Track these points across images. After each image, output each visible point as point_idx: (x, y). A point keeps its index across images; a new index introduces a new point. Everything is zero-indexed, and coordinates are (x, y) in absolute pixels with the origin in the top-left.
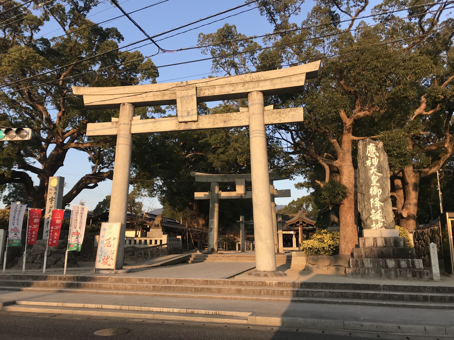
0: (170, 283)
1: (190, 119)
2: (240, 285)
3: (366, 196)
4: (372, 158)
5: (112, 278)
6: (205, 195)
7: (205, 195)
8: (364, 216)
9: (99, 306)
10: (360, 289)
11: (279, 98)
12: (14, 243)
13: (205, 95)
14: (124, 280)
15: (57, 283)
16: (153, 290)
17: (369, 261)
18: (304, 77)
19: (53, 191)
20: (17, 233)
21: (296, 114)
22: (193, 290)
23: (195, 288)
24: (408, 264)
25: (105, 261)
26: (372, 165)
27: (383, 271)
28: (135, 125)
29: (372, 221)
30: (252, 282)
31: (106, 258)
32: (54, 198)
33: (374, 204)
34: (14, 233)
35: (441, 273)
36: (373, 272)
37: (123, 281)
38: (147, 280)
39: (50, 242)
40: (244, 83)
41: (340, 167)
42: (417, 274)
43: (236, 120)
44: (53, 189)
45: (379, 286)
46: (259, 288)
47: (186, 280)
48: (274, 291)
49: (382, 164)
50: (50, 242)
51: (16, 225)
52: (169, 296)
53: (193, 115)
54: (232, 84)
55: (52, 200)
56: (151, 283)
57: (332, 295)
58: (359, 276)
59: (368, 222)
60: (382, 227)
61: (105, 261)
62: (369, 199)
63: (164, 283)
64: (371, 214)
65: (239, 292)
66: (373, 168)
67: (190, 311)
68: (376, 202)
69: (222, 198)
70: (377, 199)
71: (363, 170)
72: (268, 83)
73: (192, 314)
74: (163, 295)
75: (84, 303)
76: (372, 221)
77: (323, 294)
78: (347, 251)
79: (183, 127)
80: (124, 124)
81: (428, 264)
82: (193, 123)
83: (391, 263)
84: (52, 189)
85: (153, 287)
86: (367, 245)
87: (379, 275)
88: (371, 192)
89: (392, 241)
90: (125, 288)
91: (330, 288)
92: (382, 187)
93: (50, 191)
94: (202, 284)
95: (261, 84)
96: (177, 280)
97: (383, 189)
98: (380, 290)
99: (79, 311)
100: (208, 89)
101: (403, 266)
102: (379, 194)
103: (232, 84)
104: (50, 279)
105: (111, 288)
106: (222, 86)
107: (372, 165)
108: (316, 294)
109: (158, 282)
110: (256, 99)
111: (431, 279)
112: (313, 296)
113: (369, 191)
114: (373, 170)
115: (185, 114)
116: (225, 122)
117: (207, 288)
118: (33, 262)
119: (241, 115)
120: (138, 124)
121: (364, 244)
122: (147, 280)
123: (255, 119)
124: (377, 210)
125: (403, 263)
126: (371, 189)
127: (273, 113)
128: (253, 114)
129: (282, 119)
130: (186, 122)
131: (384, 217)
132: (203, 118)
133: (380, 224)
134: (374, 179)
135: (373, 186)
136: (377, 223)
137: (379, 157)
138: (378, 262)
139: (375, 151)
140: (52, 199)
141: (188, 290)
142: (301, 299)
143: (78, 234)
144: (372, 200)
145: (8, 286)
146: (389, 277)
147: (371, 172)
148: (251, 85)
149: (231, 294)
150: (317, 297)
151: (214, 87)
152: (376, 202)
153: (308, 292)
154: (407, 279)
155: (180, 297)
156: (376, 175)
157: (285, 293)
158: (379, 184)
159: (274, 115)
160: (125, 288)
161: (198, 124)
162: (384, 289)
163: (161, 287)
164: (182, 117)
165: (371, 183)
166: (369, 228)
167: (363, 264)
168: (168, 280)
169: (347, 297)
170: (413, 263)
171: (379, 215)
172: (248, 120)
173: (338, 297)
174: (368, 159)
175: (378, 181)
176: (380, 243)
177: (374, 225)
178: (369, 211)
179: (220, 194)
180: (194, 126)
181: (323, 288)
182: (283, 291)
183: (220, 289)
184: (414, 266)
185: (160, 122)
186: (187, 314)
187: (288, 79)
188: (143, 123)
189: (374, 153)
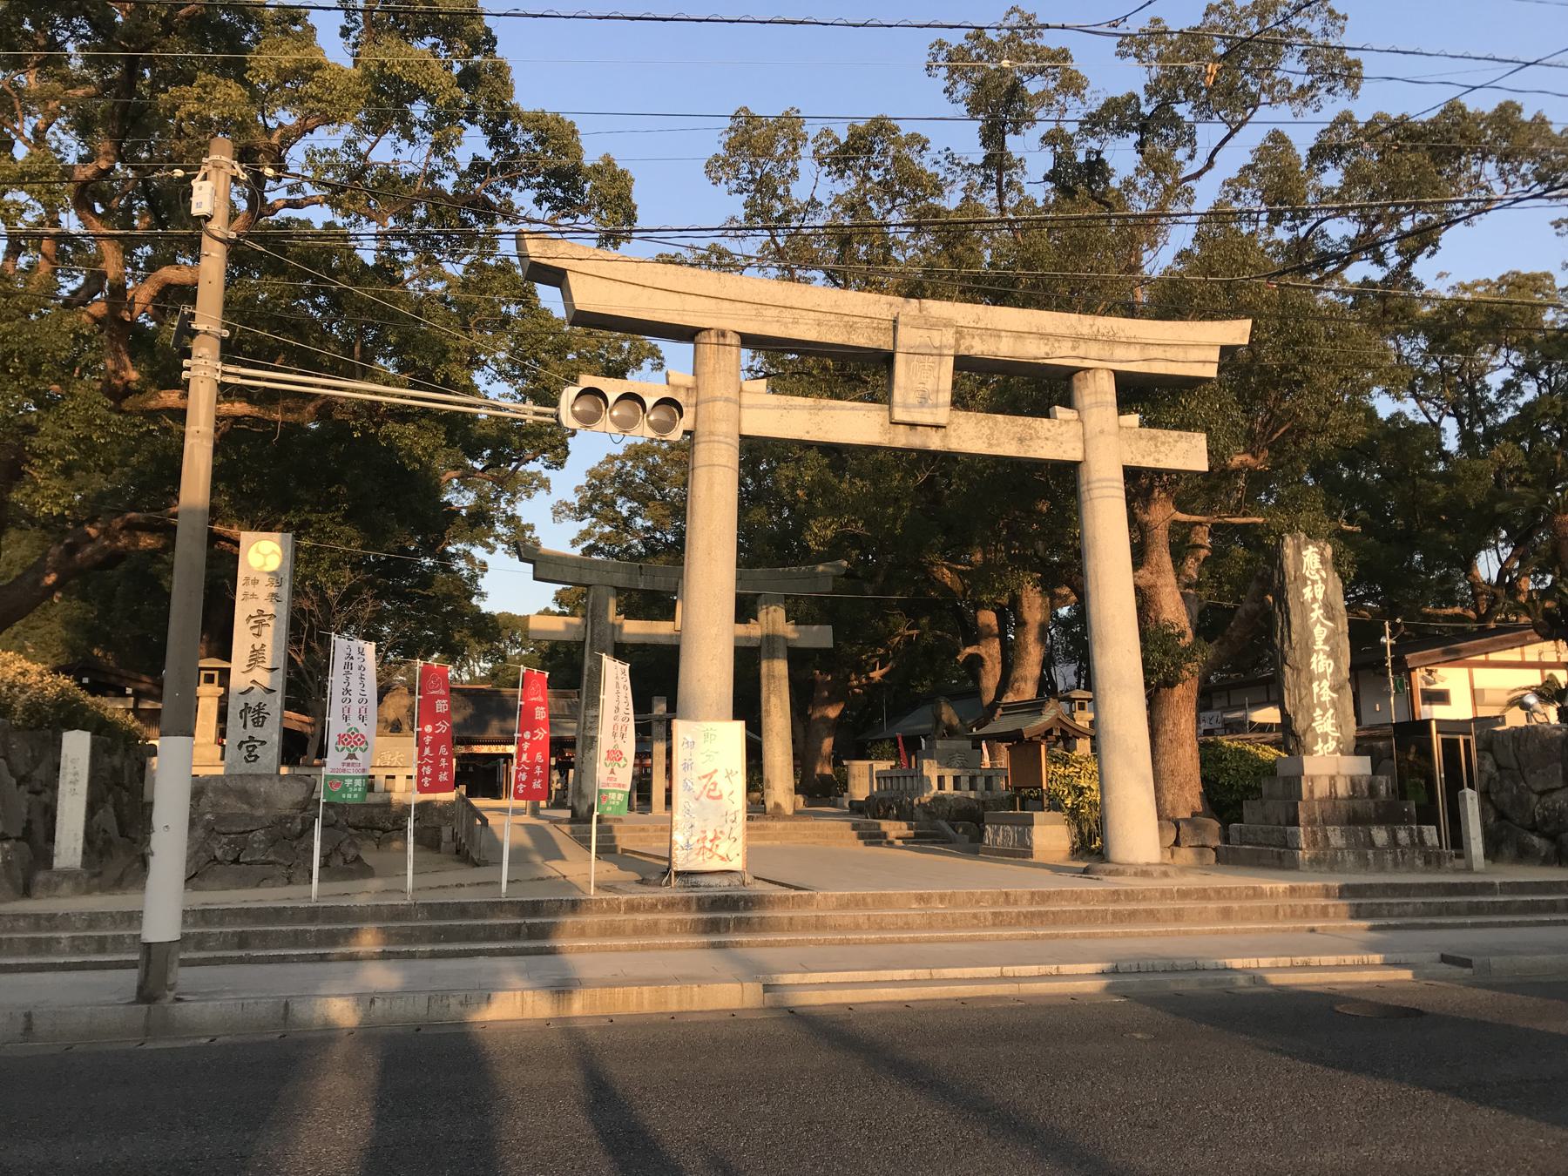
0: (1016, 903)
1: (929, 420)
2: (1202, 898)
3: (1303, 674)
4: (1314, 582)
5: (825, 897)
6: (568, 625)
7: (568, 625)
8: (1300, 725)
9: (1052, 969)
10: (1459, 894)
11: (1143, 395)
12: (345, 790)
13: (972, 352)
14: (869, 900)
15: (656, 923)
16: (994, 925)
17: (1338, 832)
18: (1215, 355)
19: (264, 590)
20: (358, 753)
21: (1186, 452)
22: (1109, 917)
23: (1115, 913)
24: (1411, 835)
25: (708, 845)
26: (1314, 599)
27: (1370, 854)
28: (751, 407)
29: (1316, 736)
30: (1230, 890)
31: (710, 836)
32: (273, 616)
33: (1319, 696)
34: (346, 753)
35: (1486, 856)
36: (1352, 857)
37: (865, 904)
38: (942, 898)
39: (521, 786)
40: (1078, 339)
41: (1150, 587)
42: (1434, 859)
43: (1046, 439)
44: (265, 580)
45: (1493, 884)
46: (1272, 904)
47: (1060, 893)
48: (1306, 907)
49: (1331, 598)
50: (521, 786)
51: (355, 721)
52: (1074, 936)
53: (936, 406)
54: (1043, 336)
55: (260, 624)
56: (956, 906)
57: (1430, 910)
58: (1324, 868)
59: (1309, 738)
60: (1334, 752)
61: (708, 845)
62: (1311, 682)
63: (995, 903)
64: (1313, 720)
65: (1226, 914)
66: (1316, 606)
67: (1299, 960)
68: (1323, 691)
69: (625, 639)
70: (1326, 684)
71: (1298, 612)
72: (1134, 353)
73: (1306, 967)
74: (1057, 936)
75: (1002, 965)
76: (1316, 736)
77: (1410, 908)
78: (1181, 809)
79: (902, 439)
80: (727, 400)
81: (1457, 839)
82: (932, 432)
83: (1380, 835)
84: (256, 582)
85: (994, 914)
86: (1317, 794)
87: (1363, 863)
88: (1313, 666)
89: (1364, 785)
90: (906, 923)
91: (1400, 896)
92: (1333, 654)
93: (251, 589)
94: (1105, 901)
95: (1120, 352)
96: (1033, 894)
97: (1336, 660)
98: (1495, 894)
99: (883, 991)
100: (980, 336)
101: (1402, 843)
102: (1330, 671)
103: (1043, 336)
104: (589, 910)
105: (857, 927)
106: (1019, 335)
107: (1314, 599)
108: (1396, 910)
109: (978, 902)
110: (1099, 392)
111: (1469, 869)
112: (1390, 915)
113: (1309, 664)
114: (1317, 613)
115: (913, 399)
116: (1021, 440)
117: (1145, 911)
118: (236, 861)
119: (1064, 428)
120: (763, 407)
121: (1311, 792)
122: (942, 898)
123: (1100, 443)
124: (1325, 711)
125: (1403, 835)
126: (1314, 659)
127: (1141, 437)
128: (1102, 432)
129: (1161, 457)
130: (913, 425)
131: (1339, 727)
132: (961, 421)
133: (1332, 745)
134: (1320, 633)
135: (1317, 652)
136: (1325, 742)
137: (1324, 581)
138: (1356, 835)
139: (1318, 565)
140: (259, 620)
141: (1096, 919)
142: (1392, 922)
143: (615, 755)
144: (1315, 685)
145: (447, 941)
146: (1382, 869)
147: (1314, 615)
148: (1094, 350)
149: (1207, 922)
150: (1400, 916)
151: (996, 333)
152: (1323, 691)
153: (1380, 905)
154: (1412, 869)
155: (1103, 937)
156: (1323, 625)
157: (1331, 910)
158: (1327, 648)
159: (1143, 443)
160: (906, 923)
161: (945, 436)
162: (1502, 892)
163: (1019, 914)
164: (906, 406)
165: (1314, 643)
166: (1311, 753)
167: (1326, 838)
168: (1007, 894)
169: (1457, 913)
170: (1420, 833)
171: (1330, 721)
172: (1080, 445)
173: (1439, 914)
174: (1305, 585)
175: (1326, 641)
176: (1342, 789)
177: (1320, 744)
178: (1310, 710)
179: (621, 626)
180: (935, 442)
181: (1387, 896)
182: (1326, 907)
183: (1179, 910)
184: (1422, 842)
185: (832, 412)
186: (1293, 968)
187: (1169, 356)
188: (778, 407)
189: (1318, 571)
